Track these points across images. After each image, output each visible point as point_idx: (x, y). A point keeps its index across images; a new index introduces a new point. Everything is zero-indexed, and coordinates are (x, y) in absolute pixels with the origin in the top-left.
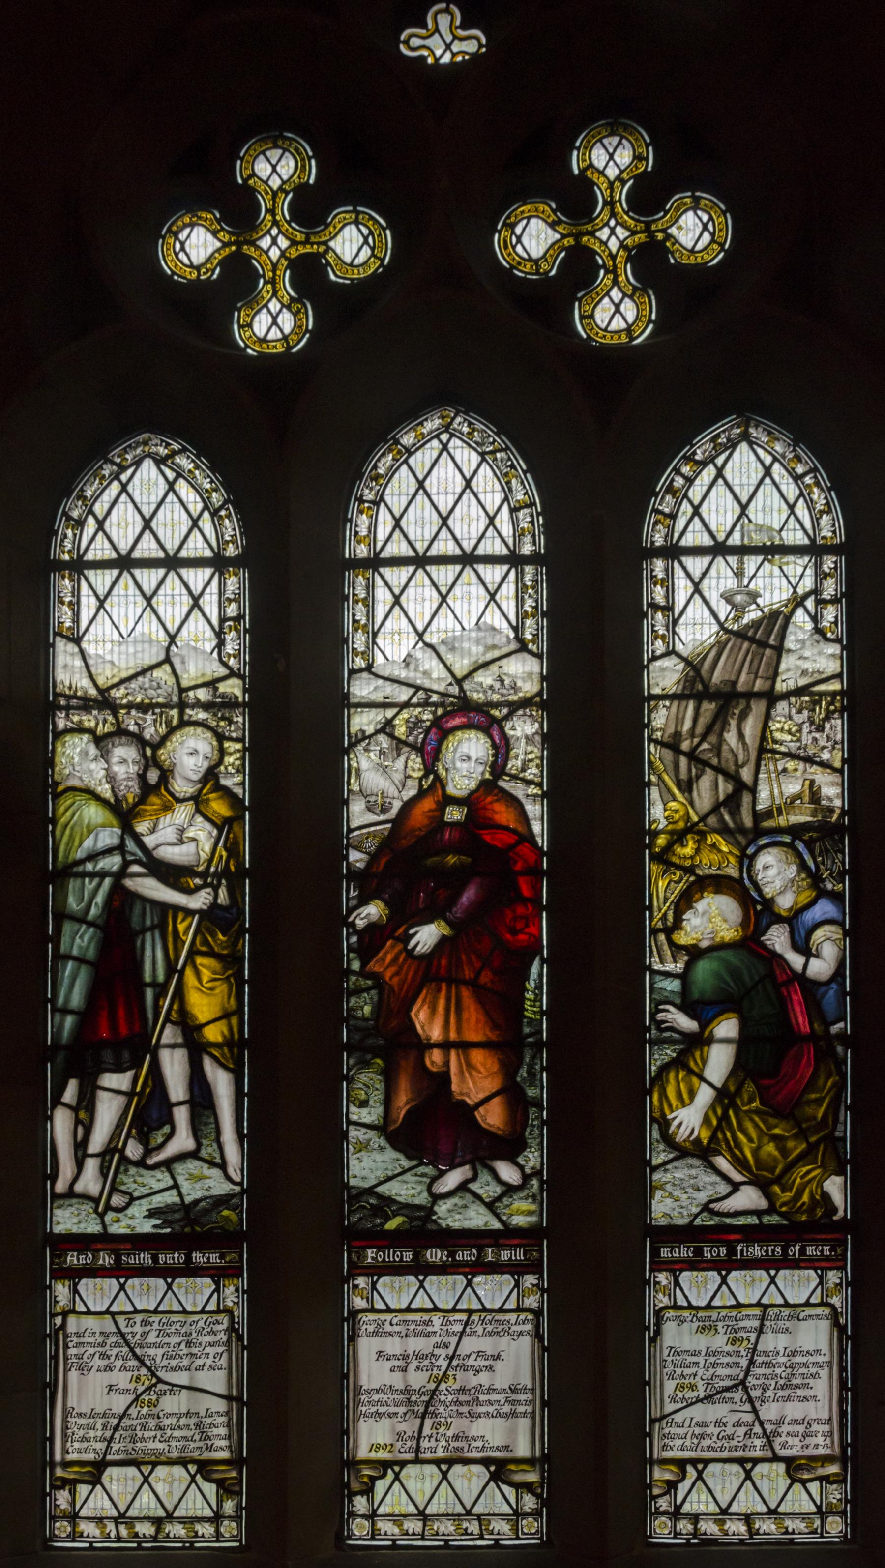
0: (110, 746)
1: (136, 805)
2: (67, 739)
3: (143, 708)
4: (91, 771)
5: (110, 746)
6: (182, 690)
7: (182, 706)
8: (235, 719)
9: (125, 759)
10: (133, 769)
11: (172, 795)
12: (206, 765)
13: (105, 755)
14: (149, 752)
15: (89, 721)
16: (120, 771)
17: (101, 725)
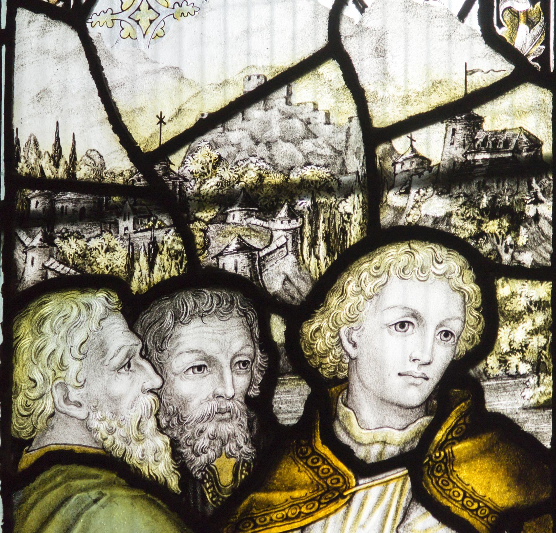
0: (169, 319)
1: (241, 490)
2: (46, 310)
3: (262, 200)
4: (115, 400)
5: (169, 319)
6: (375, 137)
7: (375, 183)
8: (531, 211)
9: (212, 347)
10: (236, 384)
11: (345, 453)
12: (442, 356)
13: (152, 350)
14: (278, 329)
15: (108, 250)
16: (196, 393)
17: (143, 262)
